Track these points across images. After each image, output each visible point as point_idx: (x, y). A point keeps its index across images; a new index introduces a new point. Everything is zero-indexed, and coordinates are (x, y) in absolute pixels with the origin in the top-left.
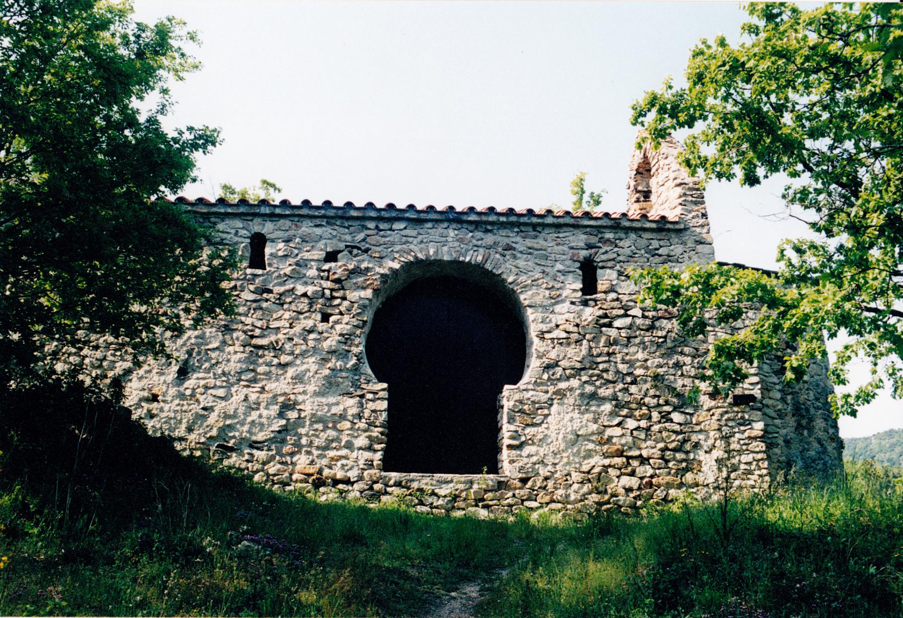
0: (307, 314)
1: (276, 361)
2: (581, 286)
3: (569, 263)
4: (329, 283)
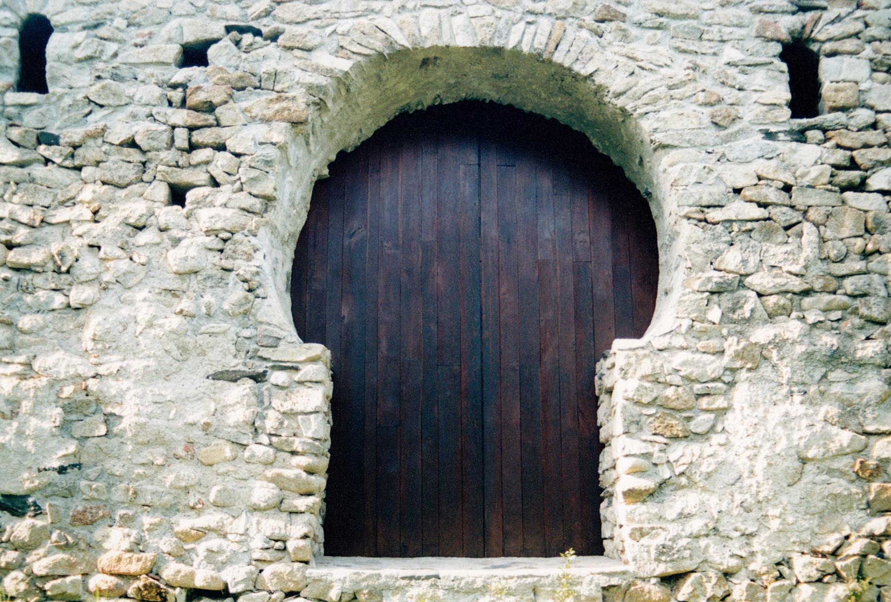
0: (136, 188)
1: (59, 300)
2: (788, 96)
3: (757, 44)
4: (184, 112)
